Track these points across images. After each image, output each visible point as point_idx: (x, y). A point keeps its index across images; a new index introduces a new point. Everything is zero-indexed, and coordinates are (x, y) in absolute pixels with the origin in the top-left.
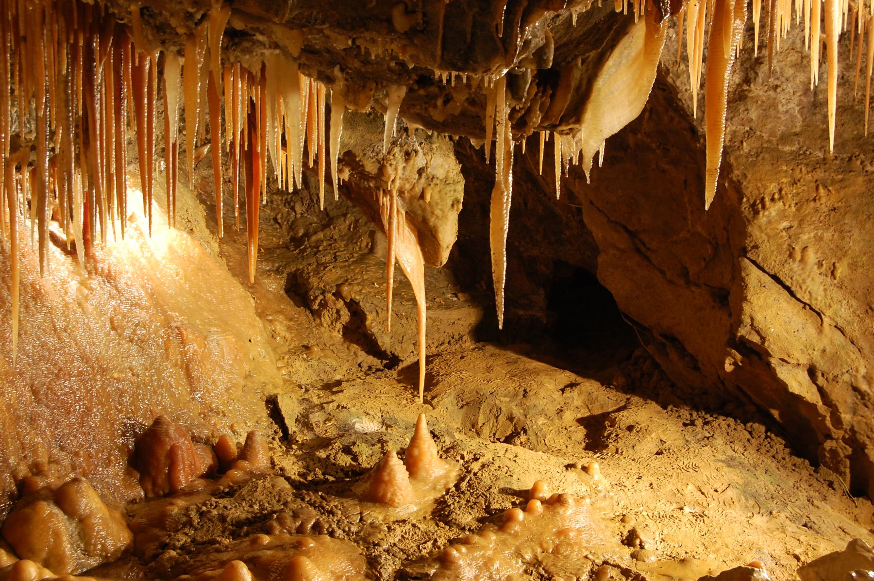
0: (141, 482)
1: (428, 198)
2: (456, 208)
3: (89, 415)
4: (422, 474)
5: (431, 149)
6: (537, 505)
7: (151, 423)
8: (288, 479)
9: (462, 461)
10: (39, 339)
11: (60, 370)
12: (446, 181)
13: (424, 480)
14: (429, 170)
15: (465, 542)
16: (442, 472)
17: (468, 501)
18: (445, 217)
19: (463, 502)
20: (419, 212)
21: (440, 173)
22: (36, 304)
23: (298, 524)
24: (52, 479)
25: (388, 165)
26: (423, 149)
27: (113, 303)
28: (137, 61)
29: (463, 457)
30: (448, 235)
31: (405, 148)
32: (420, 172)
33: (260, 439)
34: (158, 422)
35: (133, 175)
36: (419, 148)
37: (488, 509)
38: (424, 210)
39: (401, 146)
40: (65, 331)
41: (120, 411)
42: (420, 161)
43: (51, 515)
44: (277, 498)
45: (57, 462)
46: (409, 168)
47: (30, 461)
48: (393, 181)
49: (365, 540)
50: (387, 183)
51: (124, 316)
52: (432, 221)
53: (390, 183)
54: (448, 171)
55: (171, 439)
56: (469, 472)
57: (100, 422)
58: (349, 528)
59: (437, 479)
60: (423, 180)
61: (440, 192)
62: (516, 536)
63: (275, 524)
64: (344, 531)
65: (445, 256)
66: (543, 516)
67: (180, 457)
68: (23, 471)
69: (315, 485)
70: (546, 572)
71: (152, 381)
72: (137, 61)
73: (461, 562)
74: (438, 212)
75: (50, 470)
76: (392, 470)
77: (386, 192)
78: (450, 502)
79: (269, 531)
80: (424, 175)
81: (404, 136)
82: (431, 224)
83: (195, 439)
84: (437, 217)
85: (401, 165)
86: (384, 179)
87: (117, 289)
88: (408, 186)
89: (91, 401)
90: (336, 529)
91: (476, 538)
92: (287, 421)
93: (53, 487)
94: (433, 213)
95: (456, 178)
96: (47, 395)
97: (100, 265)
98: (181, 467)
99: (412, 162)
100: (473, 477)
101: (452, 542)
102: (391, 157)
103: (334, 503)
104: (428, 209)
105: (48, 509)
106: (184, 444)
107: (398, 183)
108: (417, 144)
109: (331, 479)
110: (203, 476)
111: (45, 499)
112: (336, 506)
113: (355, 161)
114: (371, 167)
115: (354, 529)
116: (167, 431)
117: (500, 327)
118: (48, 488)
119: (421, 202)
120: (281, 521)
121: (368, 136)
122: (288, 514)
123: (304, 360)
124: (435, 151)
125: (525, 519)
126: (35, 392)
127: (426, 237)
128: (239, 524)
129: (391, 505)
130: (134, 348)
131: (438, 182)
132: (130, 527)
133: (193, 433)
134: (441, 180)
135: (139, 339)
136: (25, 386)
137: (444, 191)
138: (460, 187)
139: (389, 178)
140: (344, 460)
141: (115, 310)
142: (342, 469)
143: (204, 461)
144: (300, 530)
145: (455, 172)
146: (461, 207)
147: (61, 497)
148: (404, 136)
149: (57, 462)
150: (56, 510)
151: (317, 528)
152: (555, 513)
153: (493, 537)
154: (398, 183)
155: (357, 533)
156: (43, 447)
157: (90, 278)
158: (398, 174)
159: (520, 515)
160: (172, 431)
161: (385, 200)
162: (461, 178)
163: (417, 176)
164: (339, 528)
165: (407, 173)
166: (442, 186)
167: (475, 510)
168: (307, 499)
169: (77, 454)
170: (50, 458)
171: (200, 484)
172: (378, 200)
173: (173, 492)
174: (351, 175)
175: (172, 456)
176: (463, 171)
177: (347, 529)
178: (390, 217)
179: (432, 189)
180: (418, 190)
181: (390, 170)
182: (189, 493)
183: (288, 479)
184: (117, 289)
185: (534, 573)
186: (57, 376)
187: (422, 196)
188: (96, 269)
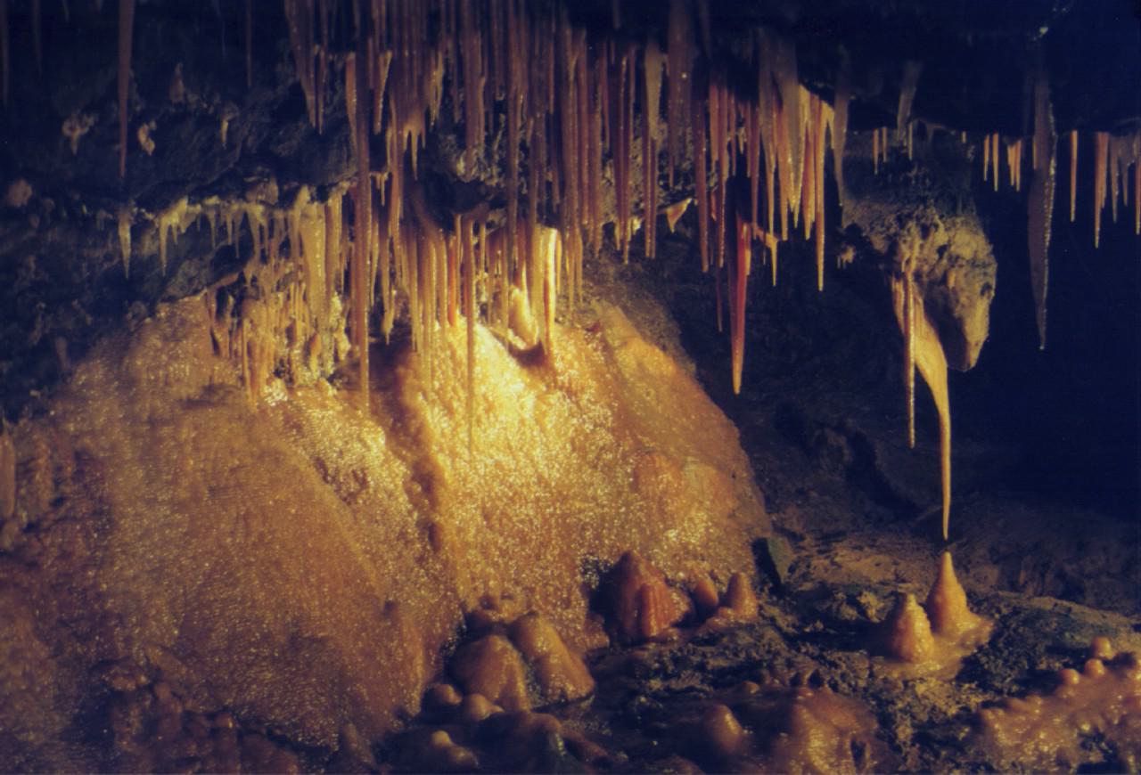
0: (607, 629)
1: (951, 282)
2: (986, 294)
3: (546, 547)
4: (948, 627)
5: (954, 224)
6: (1098, 668)
7: (618, 559)
8: (779, 629)
9: (997, 616)
10: (492, 457)
11: (515, 493)
12: (973, 263)
13: (950, 637)
14: (953, 248)
15: (1004, 705)
16: (972, 626)
17: (1006, 661)
18: (972, 305)
19: (1000, 662)
20: (940, 301)
21: (967, 253)
22: (488, 417)
23: (792, 674)
24: (506, 612)
25: (901, 242)
26: (944, 223)
27: (575, 421)
28: (613, 59)
29: (999, 611)
30: (977, 329)
31: (923, 221)
32: (942, 250)
33: (745, 582)
34: (626, 558)
35: (610, 166)
36: (939, 222)
37: (1032, 670)
38: (946, 297)
39: (918, 219)
40: (521, 449)
41: (582, 546)
42: (940, 237)
43: (504, 651)
44: (767, 648)
45: (510, 597)
46: (927, 246)
47: (482, 592)
48: (908, 262)
49: (875, 696)
50: (900, 264)
51: (586, 436)
52: (957, 312)
53: (903, 264)
54: (976, 252)
55: (641, 577)
56: (1008, 628)
57: (559, 555)
58: (856, 683)
59: (967, 634)
60: (945, 261)
61: (966, 275)
62: (1069, 702)
63: (765, 672)
64: (850, 685)
65: (974, 356)
66: (1102, 680)
67: (651, 598)
68: (472, 604)
69: (813, 638)
70: (1111, 748)
71: (618, 513)
72: (613, 59)
73: (997, 726)
74: (963, 299)
75: (503, 605)
76: (909, 617)
77: (900, 276)
78: (984, 660)
79: (758, 680)
80: (946, 254)
81: (921, 207)
82: (956, 315)
83: (669, 583)
84: (963, 306)
85: (918, 242)
86: (897, 259)
87: (579, 406)
88: (926, 268)
89: (549, 531)
90: (840, 682)
91: (1016, 702)
92: (779, 569)
93: (507, 622)
94: (958, 301)
95: (987, 260)
96: (500, 520)
97: (560, 378)
98: (653, 611)
99: (931, 238)
100: (1012, 633)
101: (986, 705)
102: (905, 232)
103: (835, 655)
104: (952, 296)
105: (500, 643)
106: (656, 583)
107: (914, 265)
108: (937, 217)
109: (832, 632)
110: (676, 625)
111: (497, 634)
112: (840, 659)
113: (861, 237)
114: (879, 244)
115: (862, 684)
116: (636, 568)
117: (1073, 218)
118: (501, 622)
119: (942, 288)
120: (771, 668)
121: (876, 207)
122: (779, 662)
123: (798, 506)
124: (958, 226)
125: (1081, 682)
126: (487, 517)
127: (949, 332)
128: (721, 672)
129: (909, 661)
130: (598, 475)
131: (964, 263)
132: (594, 674)
133: (666, 576)
134: (968, 261)
135: (605, 465)
136: (475, 509)
137: (970, 275)
138: (992, 270)
139: (903, 257)
140: (849, 613)
141: (576, 430)
142: (847, 622)
143: (681, 605)
144: (796, 681)
145: (986, 252)
146: (993, 293)
147: (516, 633)
148: (921, 207)
149: (510, 597)
150: (509, 646)
151: (816, 681)
152: (1122, 677)
153: (1039, 701)
154: (914, 265)
155: (865, 689)
156: (495, 579)
157: (548, 392)
158: (914, 253)
159: (1075, 677)
160: (642, 568)
161: (898, 287)
162: (992, 259)
163: (937, 256)
164: (844, 681)
165: (926, 251)
166: (969, 268)
167: (1016, 671)
168: (804, 650)
169: (532, 590)
170: (503, 593)
171: (675, 634)
172: (889, 285)
173: (642, 639)
174: (856, 257)
175: (641, 600)
176: (995, 252)
177: (853, 683)
178: (906, 307)
179: (957, 272)
180: (939, 272)
181: (904, 248)
182: (663, 640)
183: (779, 629)
184: (579, 406)
185: (1094, 747)
186: (512, 499)
187: (944, 280)
188: (555, 381)
